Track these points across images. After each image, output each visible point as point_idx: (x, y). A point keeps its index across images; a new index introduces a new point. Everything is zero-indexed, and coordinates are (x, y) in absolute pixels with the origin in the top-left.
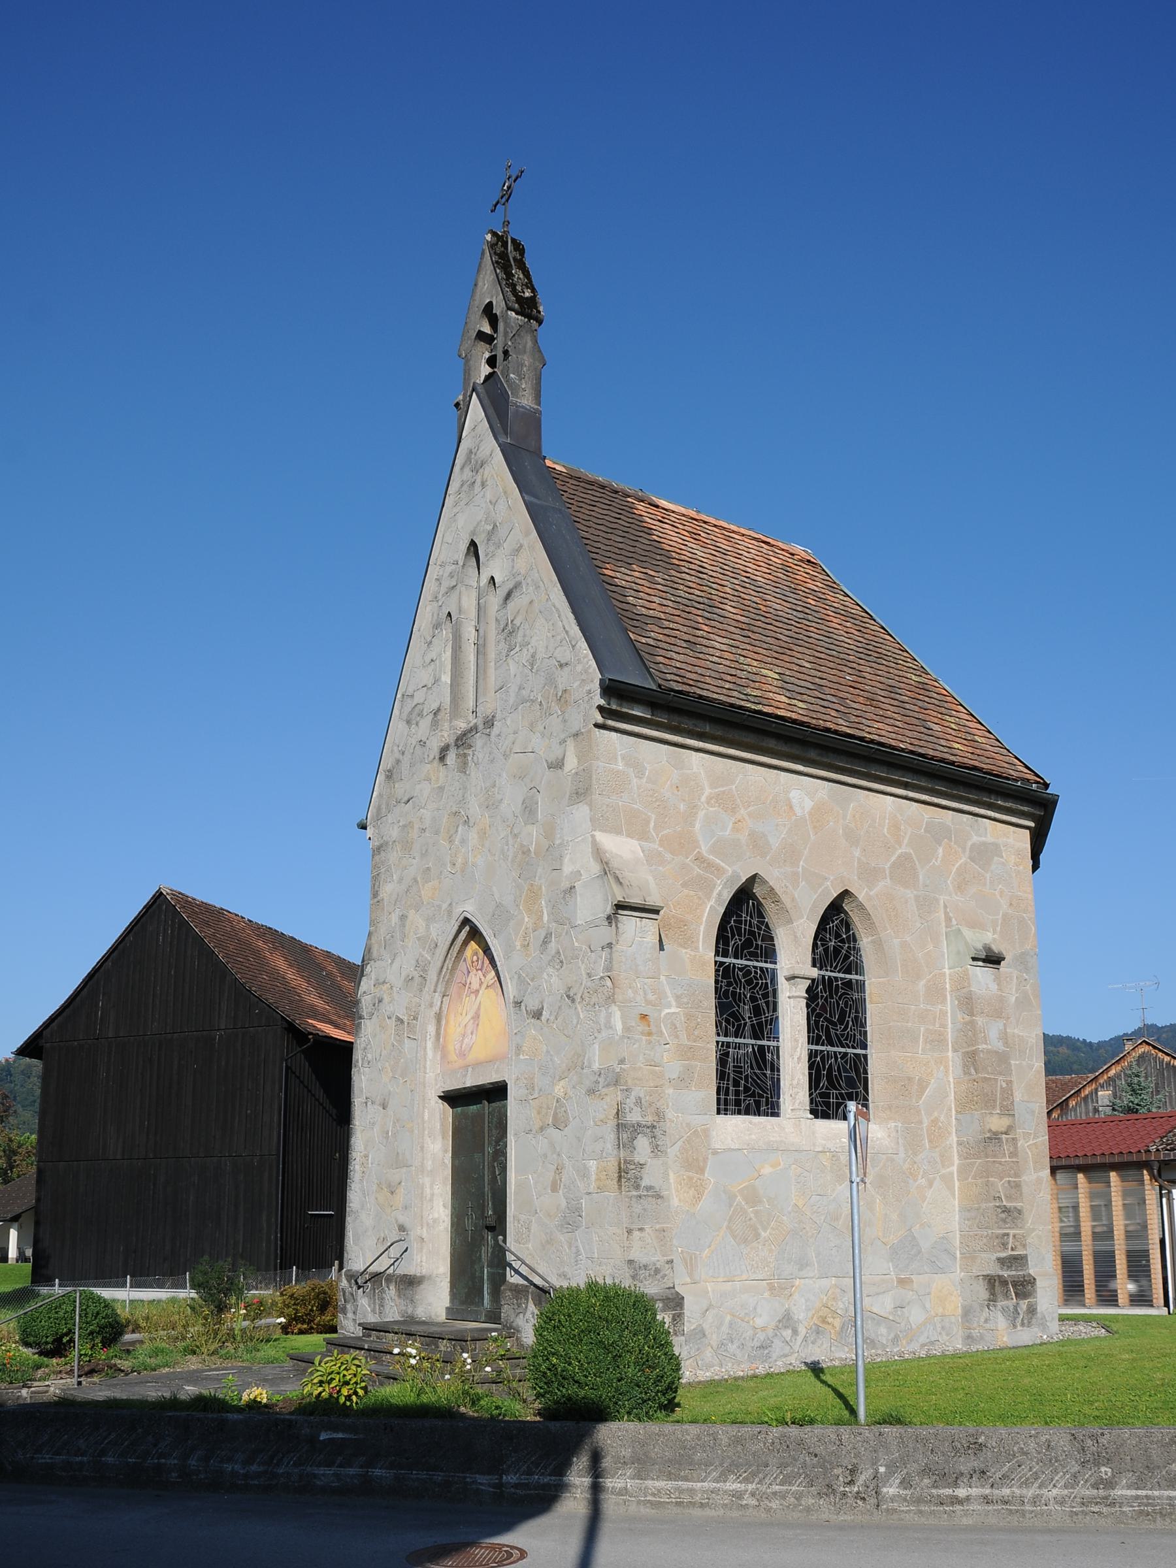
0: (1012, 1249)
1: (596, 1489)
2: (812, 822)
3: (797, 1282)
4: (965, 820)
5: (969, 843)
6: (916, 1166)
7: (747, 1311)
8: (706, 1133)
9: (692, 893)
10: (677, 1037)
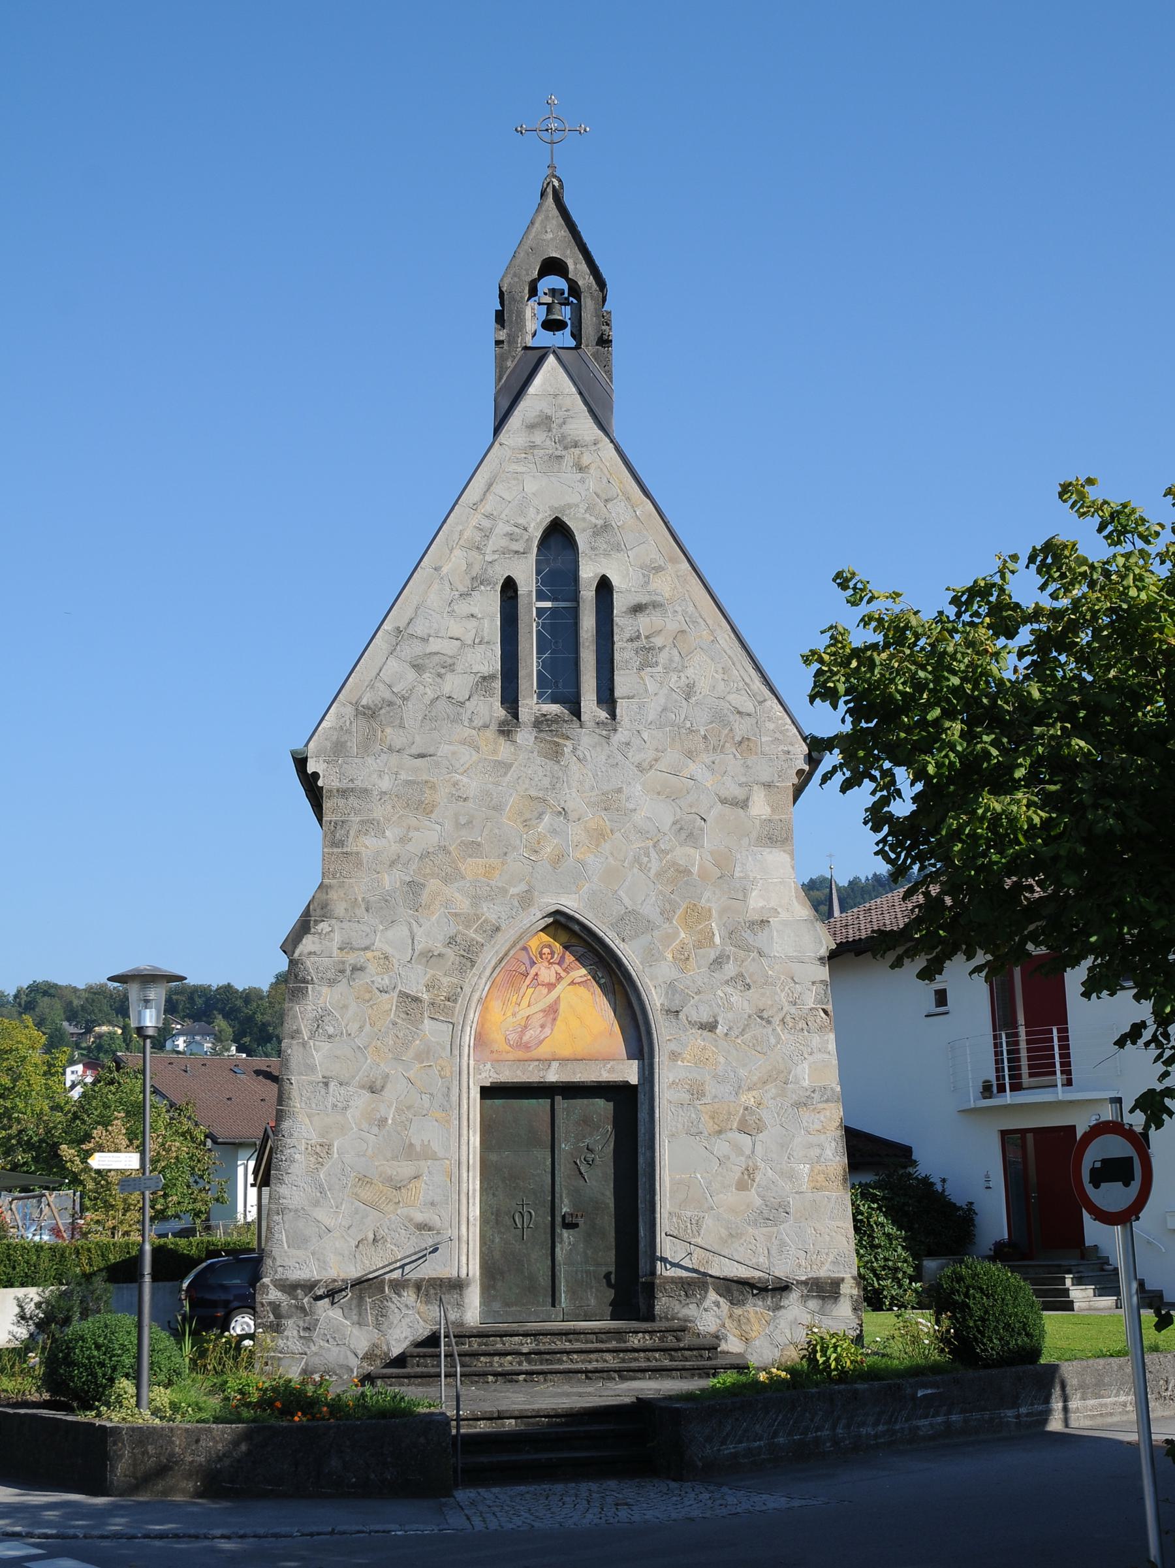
1: (1066, 1409)
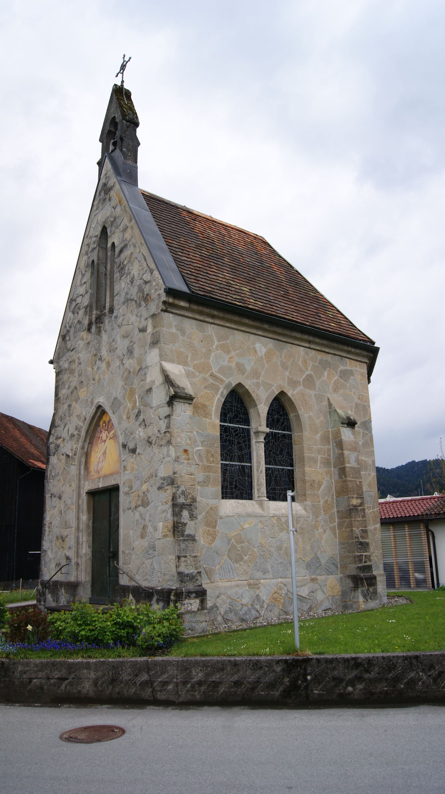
2: (266, 359)
3: (262, 581)
5: (339, 370)
6: (317, 523)
7: (238, 596)
9: (209, 392)
10: (202, 461)
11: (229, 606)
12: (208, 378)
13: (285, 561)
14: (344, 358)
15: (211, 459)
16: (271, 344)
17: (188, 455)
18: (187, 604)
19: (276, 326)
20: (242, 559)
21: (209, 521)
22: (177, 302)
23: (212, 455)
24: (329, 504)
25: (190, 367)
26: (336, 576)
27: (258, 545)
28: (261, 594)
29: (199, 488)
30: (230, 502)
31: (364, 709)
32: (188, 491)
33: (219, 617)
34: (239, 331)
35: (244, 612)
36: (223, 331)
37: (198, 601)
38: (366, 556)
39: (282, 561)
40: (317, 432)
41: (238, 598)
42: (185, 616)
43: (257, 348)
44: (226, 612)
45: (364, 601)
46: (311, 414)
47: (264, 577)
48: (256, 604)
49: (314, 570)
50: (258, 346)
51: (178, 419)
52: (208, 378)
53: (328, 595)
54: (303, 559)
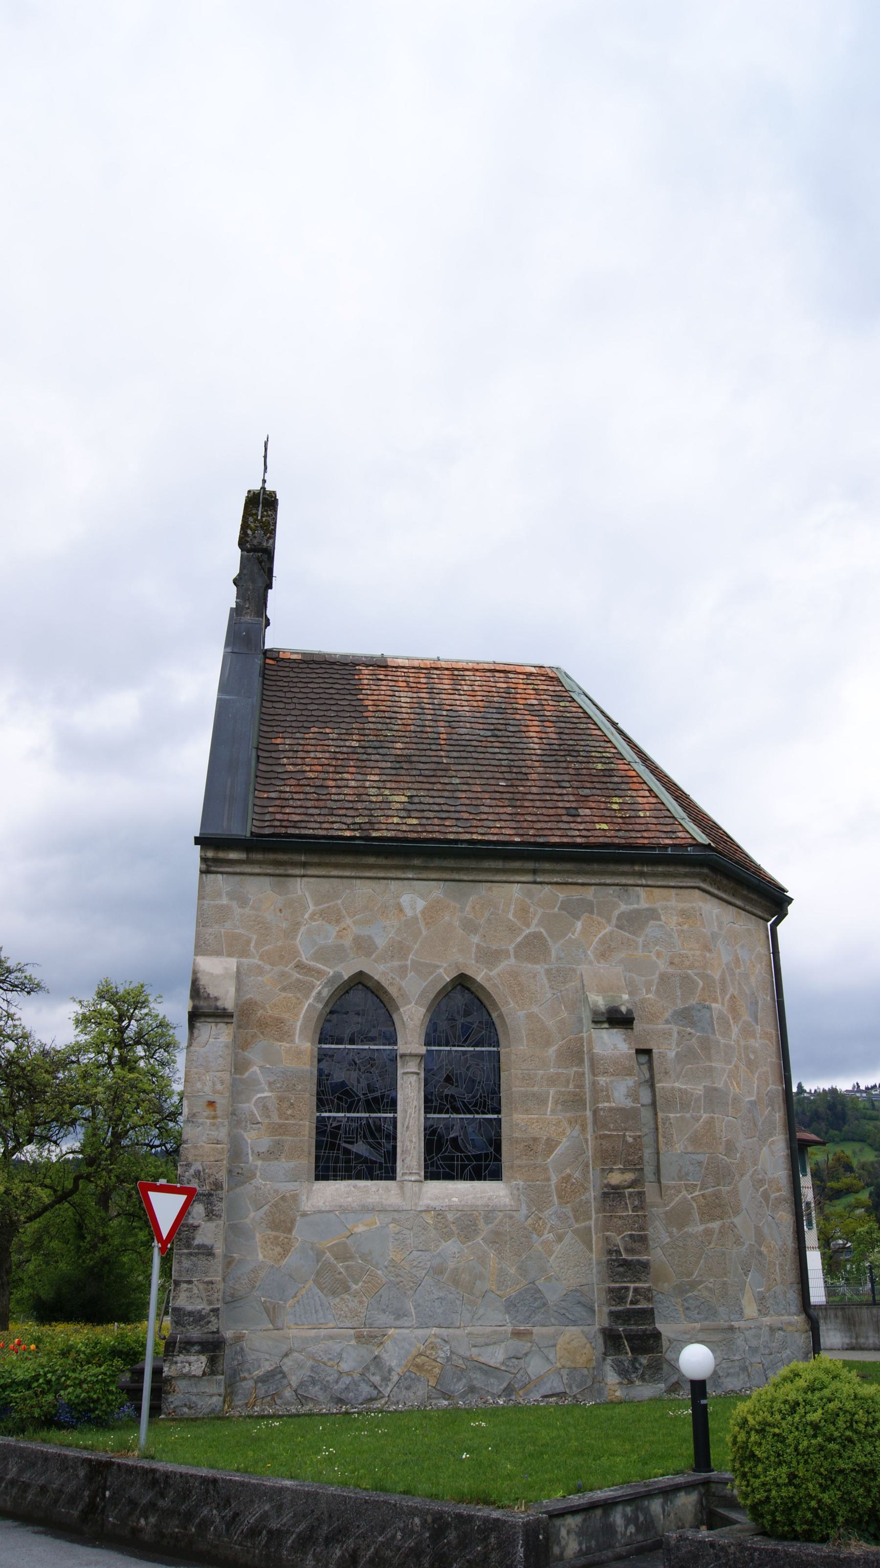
0: (632, 1303)
2: (425, 919)
3: (391, 1331)
4: (611, 892)
5: (616, 913)
6: (541, 1222)
7: (330, 1356)
8: (295, 1198)
9: (291, 995)
10: (269, 1117)
11: (309, 1373)
12: (291, 971)
13: (450, 1296)
14: (630, 888)
15: (289, 1112)
16: (436, 890)
17: (215, 1110)
18: (182, 1362)
19: (440, 858)
20: (347, 1289)
21: (277, 1221)
22: (221, 855)
23: (292, 1104)
24: (573, 1184)
25: (254, 957)
26: (586, 1328)
27: (386, 1264)
28: (385, 1356)
29: (259, 1163)
30: (337, 1186)
31: (120, 1556)
32: (207, 1171)
33: (286, 1392)
34: (363, 880)
35: (344, 1386)
36: (325, 885)
37: (203, 1359)
38: (636, 1290)
39: (441, 1294)
40: (548, 1043)
41: (330, 1359)
42: (178, 1382)
43: (404, 904)
44: (302, 1384)
45: (620, 1383)
46: (535, 1009)
47: (398, 1323)
48: (373, 1374)
49: (527, 1314)
50: (405, 900)
51: (202, 1050)
52: (291, 971)
53: (558, 1365)
54: (499, 1293)
